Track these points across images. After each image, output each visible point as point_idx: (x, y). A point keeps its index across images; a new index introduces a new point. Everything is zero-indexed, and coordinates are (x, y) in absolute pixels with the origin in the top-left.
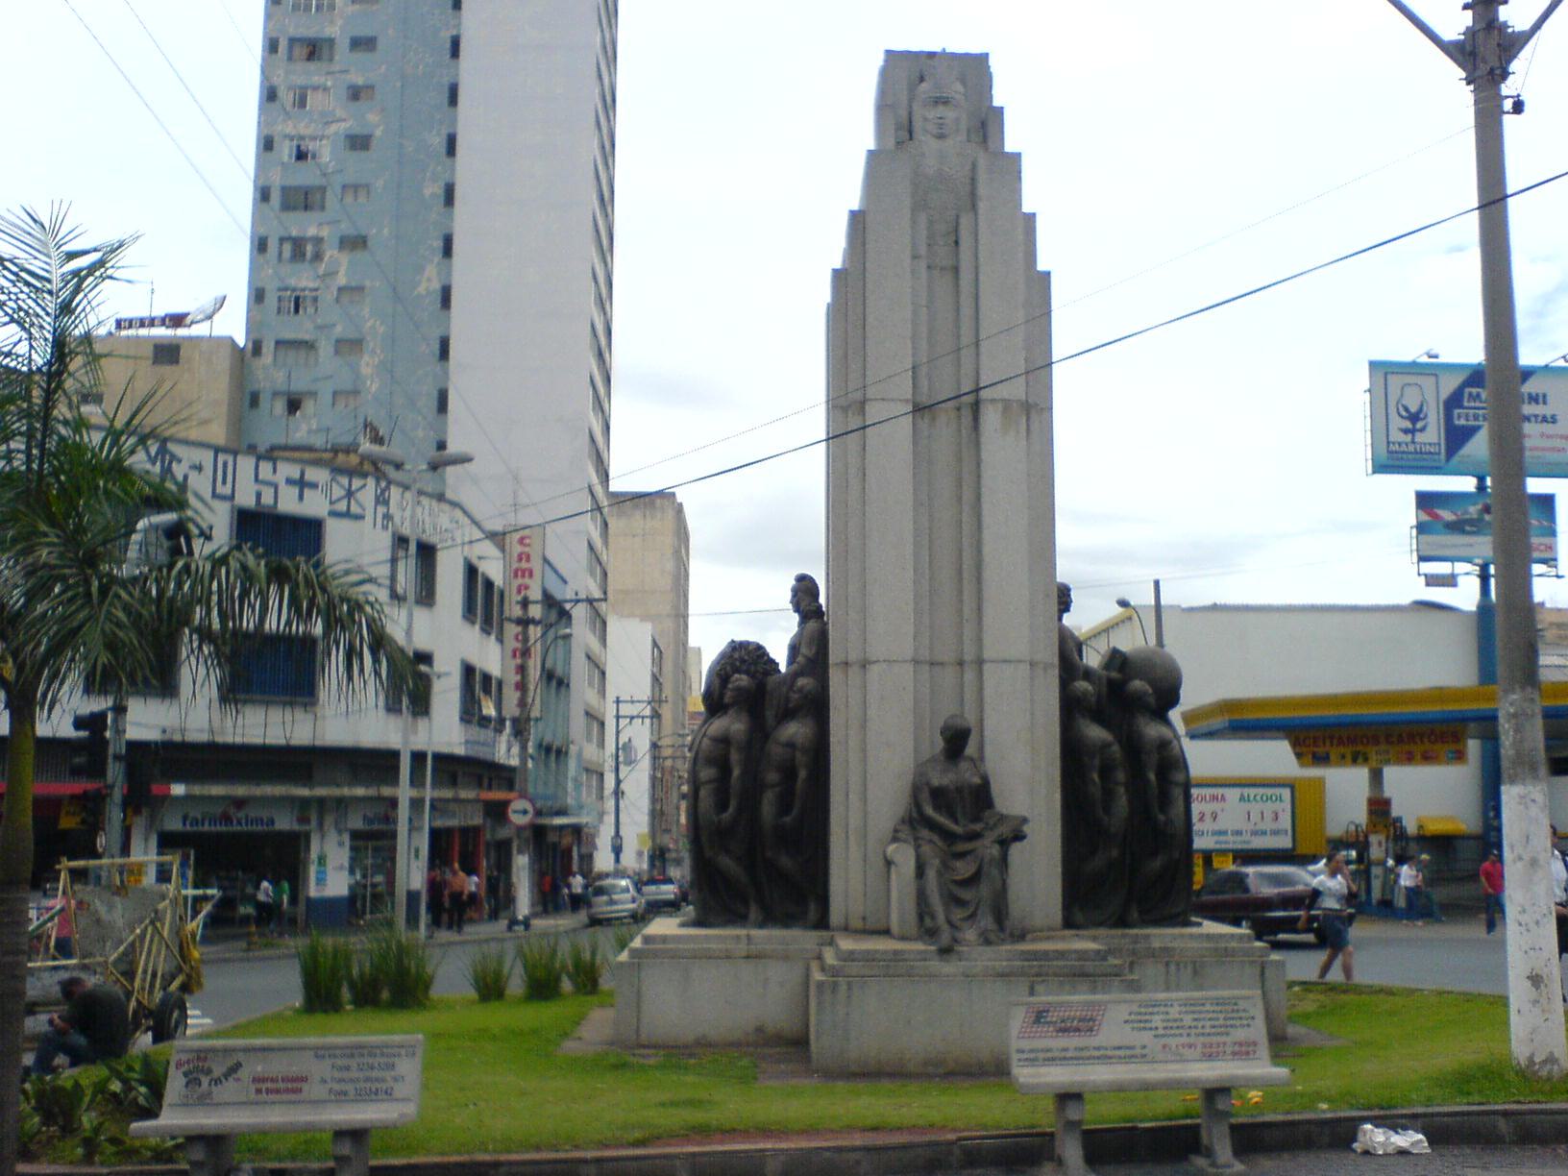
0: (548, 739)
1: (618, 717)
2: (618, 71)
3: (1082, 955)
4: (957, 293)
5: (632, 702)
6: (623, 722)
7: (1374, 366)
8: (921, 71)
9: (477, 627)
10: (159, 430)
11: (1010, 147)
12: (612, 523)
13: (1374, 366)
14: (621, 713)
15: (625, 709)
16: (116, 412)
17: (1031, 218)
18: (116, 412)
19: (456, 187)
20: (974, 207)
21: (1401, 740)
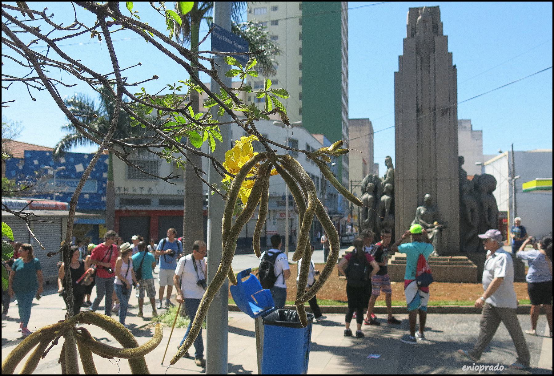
0: (331, 192)
1: (351, 186)
2: (349, 22)
3: (20, 204)
4: (430, 76)
5: (355, 181)
6: (353, 187)
7: (481, 131)
8: (306, 143)
9: (310, 162)
10: (267, 41)
11: (445, 34)
12: (350, 128)
13: (481, 131)
14: (352, 185)
15: (354, 184)
16: (188, 370)
17: (451, 54)
18: (188, 370)
19: (298, 82)
20: (434, 52)
21: (264, 245)
